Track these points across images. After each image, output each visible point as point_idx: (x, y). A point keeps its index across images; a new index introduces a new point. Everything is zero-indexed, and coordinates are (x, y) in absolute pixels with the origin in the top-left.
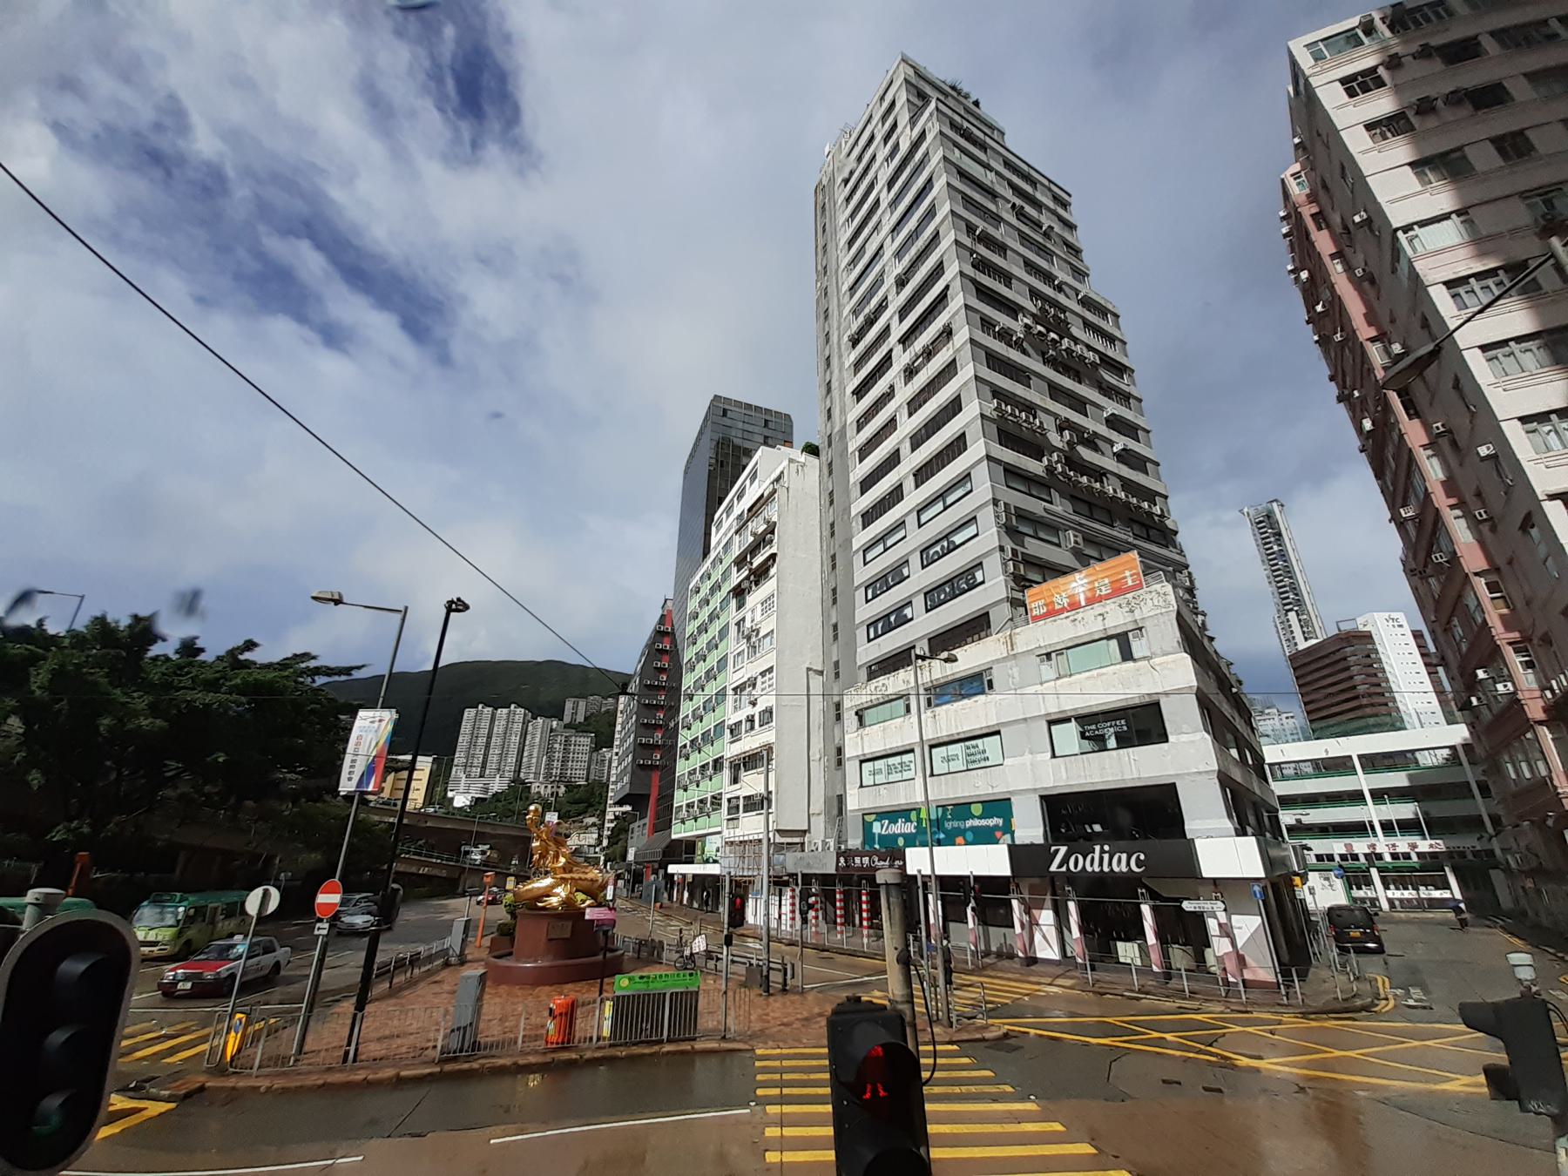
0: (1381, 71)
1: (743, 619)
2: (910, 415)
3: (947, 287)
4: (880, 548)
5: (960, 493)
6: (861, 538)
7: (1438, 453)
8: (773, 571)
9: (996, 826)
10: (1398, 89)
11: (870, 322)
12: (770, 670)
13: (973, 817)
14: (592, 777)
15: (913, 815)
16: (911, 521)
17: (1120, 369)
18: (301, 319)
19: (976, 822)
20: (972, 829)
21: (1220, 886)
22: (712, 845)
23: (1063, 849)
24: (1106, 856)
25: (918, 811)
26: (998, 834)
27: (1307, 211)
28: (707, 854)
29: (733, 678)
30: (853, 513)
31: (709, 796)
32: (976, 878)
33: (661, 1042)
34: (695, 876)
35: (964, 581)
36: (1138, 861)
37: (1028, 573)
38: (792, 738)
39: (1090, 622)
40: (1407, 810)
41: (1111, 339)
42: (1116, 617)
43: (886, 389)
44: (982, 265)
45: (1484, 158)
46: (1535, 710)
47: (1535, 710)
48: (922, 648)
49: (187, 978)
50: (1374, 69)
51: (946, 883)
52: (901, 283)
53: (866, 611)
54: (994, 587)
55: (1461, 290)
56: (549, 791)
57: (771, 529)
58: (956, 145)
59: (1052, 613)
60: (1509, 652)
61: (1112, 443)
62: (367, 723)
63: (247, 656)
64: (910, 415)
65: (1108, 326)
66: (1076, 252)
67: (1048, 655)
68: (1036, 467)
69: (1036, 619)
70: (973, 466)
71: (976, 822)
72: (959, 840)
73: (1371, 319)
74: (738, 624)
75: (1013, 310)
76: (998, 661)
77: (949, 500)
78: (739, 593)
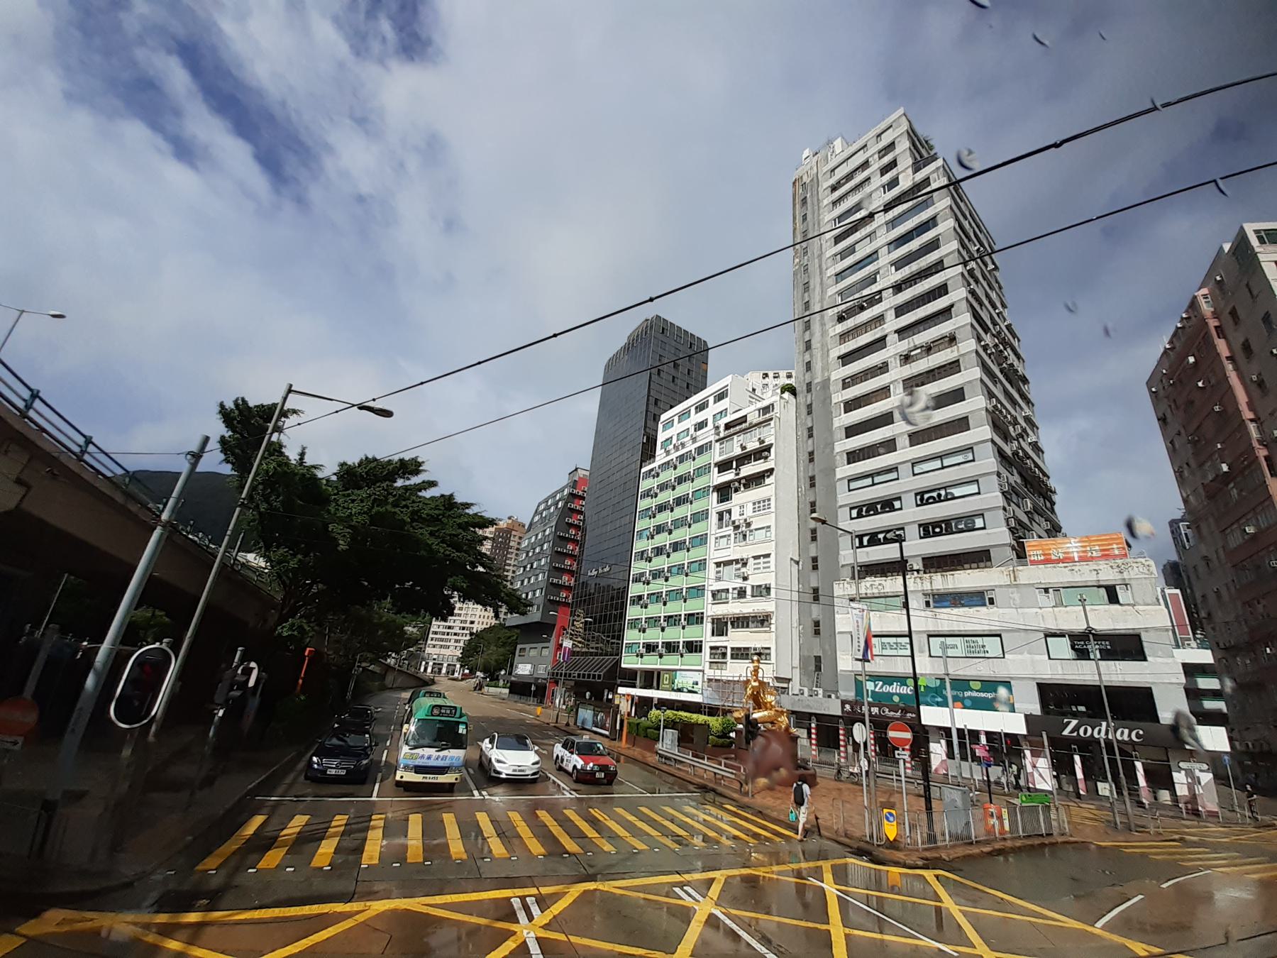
1: (729, 512)
3: (952, 306)
4: (869, 481)
5: (960, 459)
8: (768, 481)
12: (768, 556)
13: (972, 690)
18: (155, 125)
20: (970, 698)
23: (1074, 722)
27: (1213, 323)
29: (714, 553)
32: (1006, 734)
34: (640, 697)
36: (1138, 736)
39: (1085, 574)
42: (1108, 574)
54: (996, 534)
59: (1047, 561)
66: (1000, 288)
68: (1008, 450)
71: (975, 694)
73: (1251, 406)
74: (721, 515)
76: (1001, 586)
78: (724, 492)
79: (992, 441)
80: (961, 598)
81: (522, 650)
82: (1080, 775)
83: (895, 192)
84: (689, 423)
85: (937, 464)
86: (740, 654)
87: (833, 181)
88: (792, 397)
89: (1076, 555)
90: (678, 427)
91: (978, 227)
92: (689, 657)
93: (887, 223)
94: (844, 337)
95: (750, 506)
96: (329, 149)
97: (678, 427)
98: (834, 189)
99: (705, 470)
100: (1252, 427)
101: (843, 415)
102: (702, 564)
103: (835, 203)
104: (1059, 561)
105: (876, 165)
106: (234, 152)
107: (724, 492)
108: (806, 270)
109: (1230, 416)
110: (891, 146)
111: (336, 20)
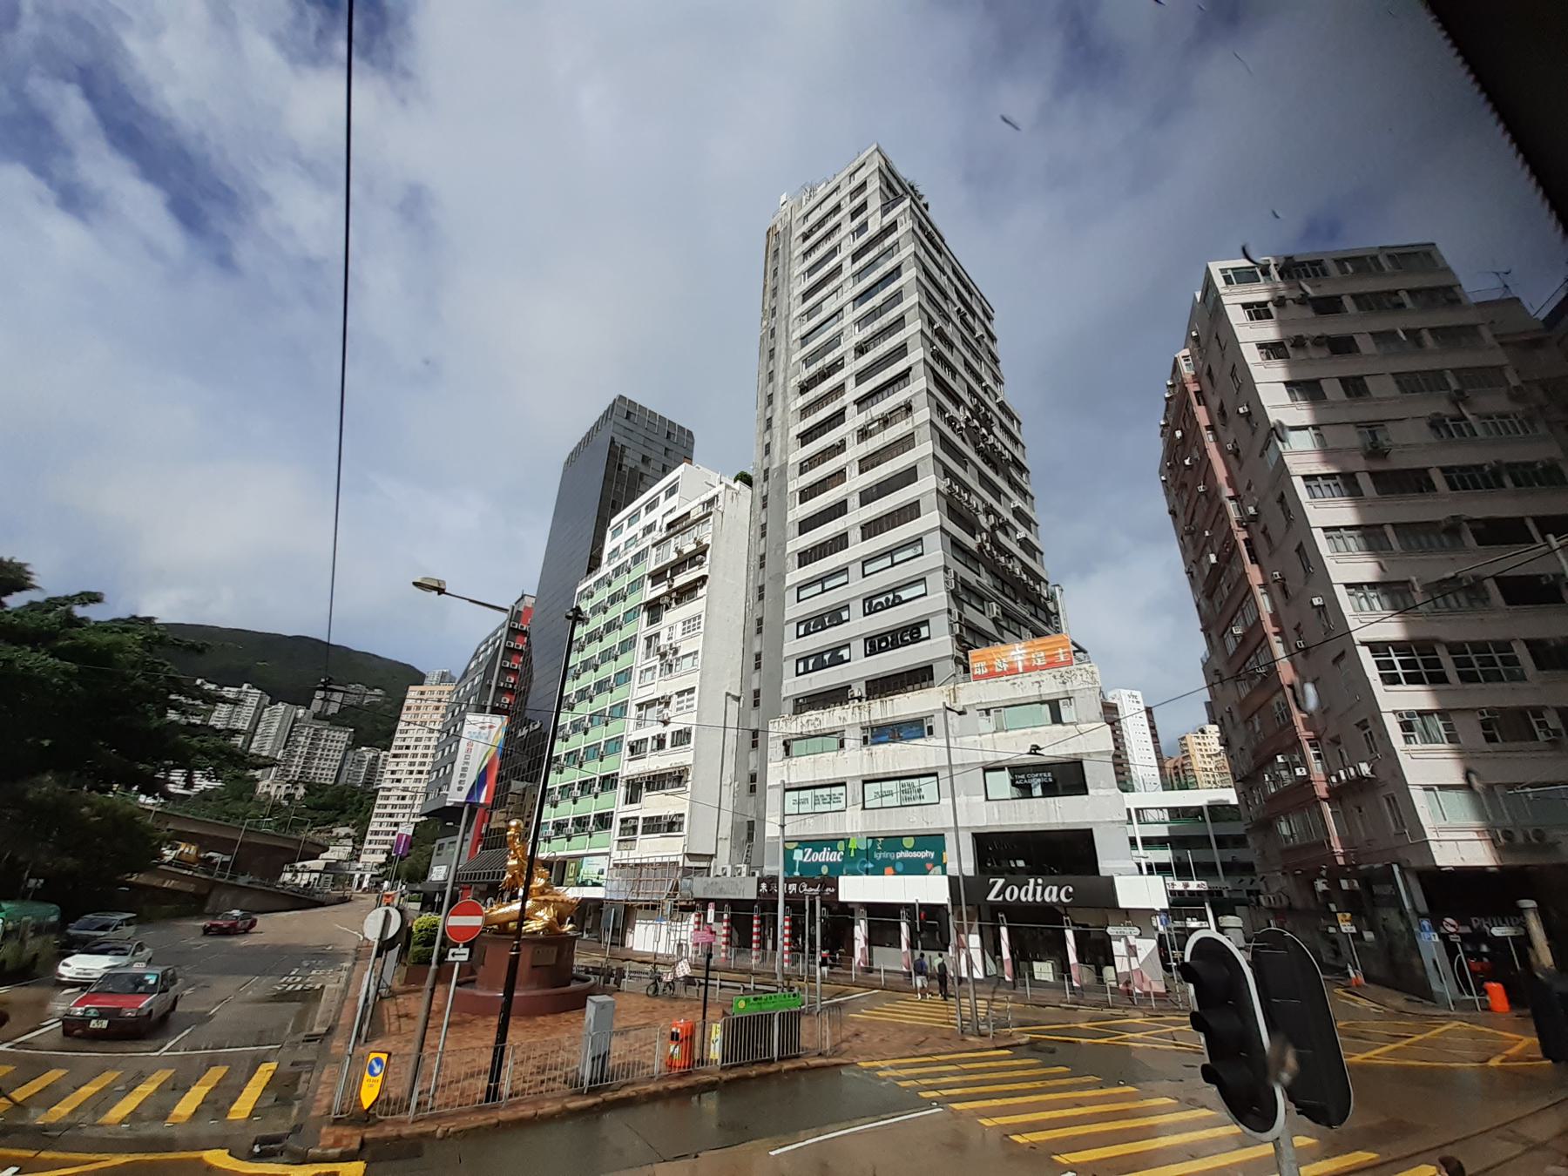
0: (1270, 306)
1: (657, 635)
2: (861, 472)
3: (910, 369)
4: (818, 588)
5: (909, 553)
6: (796, 575)
7: (1269, 593)
8: (700, 592)
9: (928, 859)
10: (1281, 324)
11: (824, 375)
12: (691, 691)
13: (905, 849)
14: (342, 781)
15: (841, 845)
16: (855, 570)
17: (1022, 469)
19: (907, 854)
20: (903, 860)
21: (1130, 916)
22: (590, 869)
23: (1001, 882)
24: (1039, 889)
25: (847, 841)
26: (929, 866)
27: (1193, 388)
28: (584, 875)
29: (638, 692)
30: (789, 550)
31: (592, 814)
32: (921, 906)
33: (772, 1061)
35: (911, 633)
36: (1068, 895)
37: (969, 638)
38: (710, 761)
39: (1027, 687)
40: (1165, 856)
41: (1016, 442)
42: (1051, 686)
43: (837, 442)
44: (938, 356)
45: (1333, 391)
46: (1321, 790)
47: (1321, 790)
48: (859, 689)
49: (102, 1015)
50: (1265, 304)
51: (873, 909)
52: (861, 350)
53: (795, 646)
54: (938, 645)
55: (1312, 484)
56: (282, 792)
57: (702, 550)
58: (922, 243)
59: (992, 674)
60: (1306, 745)
61: (1016, 531)
62: (477, 729)
63: (79, 611)
64: (861, 472)
65: (1014, 429)
66: (996, 361)
67: (987, 711)
68: (971, 543)
69: (978, 678)
70: (926, 533)
71: (907, 854)
72: (889, 869)
73: (1231, 481)
74: (649, 639)
75: (957, 401)
77: (897, 558)
78: (655, 609)
79: (942, 529)
80: (900, 730)
81: (441, 847)
82: (1006, 954)
83: (864, 238)
84: (637, 528)
85: (887, 561)
86: (653, 825)
87: (805, 228)
88: (745, 488)
89: (1020, 665)
90: (627, 533)
91: (966, 287)
92: (599, 837)
93: (854, 276)
94: (805, 411)
95: (680, 626)
96: (266, 198)
97: (627, 533)
98: (806, 237)
99: (636, 585)
100: (1231, 506)
101: (798, 507)
102: (623, 707)
103: (806, 254)
104: (1002, 674)
105: (847, 209)
106: (139, 201)
107: (655, 609)
108: (773, 335)
109: (1212, 494)
110: (863, 186)
111: (279, 40)
